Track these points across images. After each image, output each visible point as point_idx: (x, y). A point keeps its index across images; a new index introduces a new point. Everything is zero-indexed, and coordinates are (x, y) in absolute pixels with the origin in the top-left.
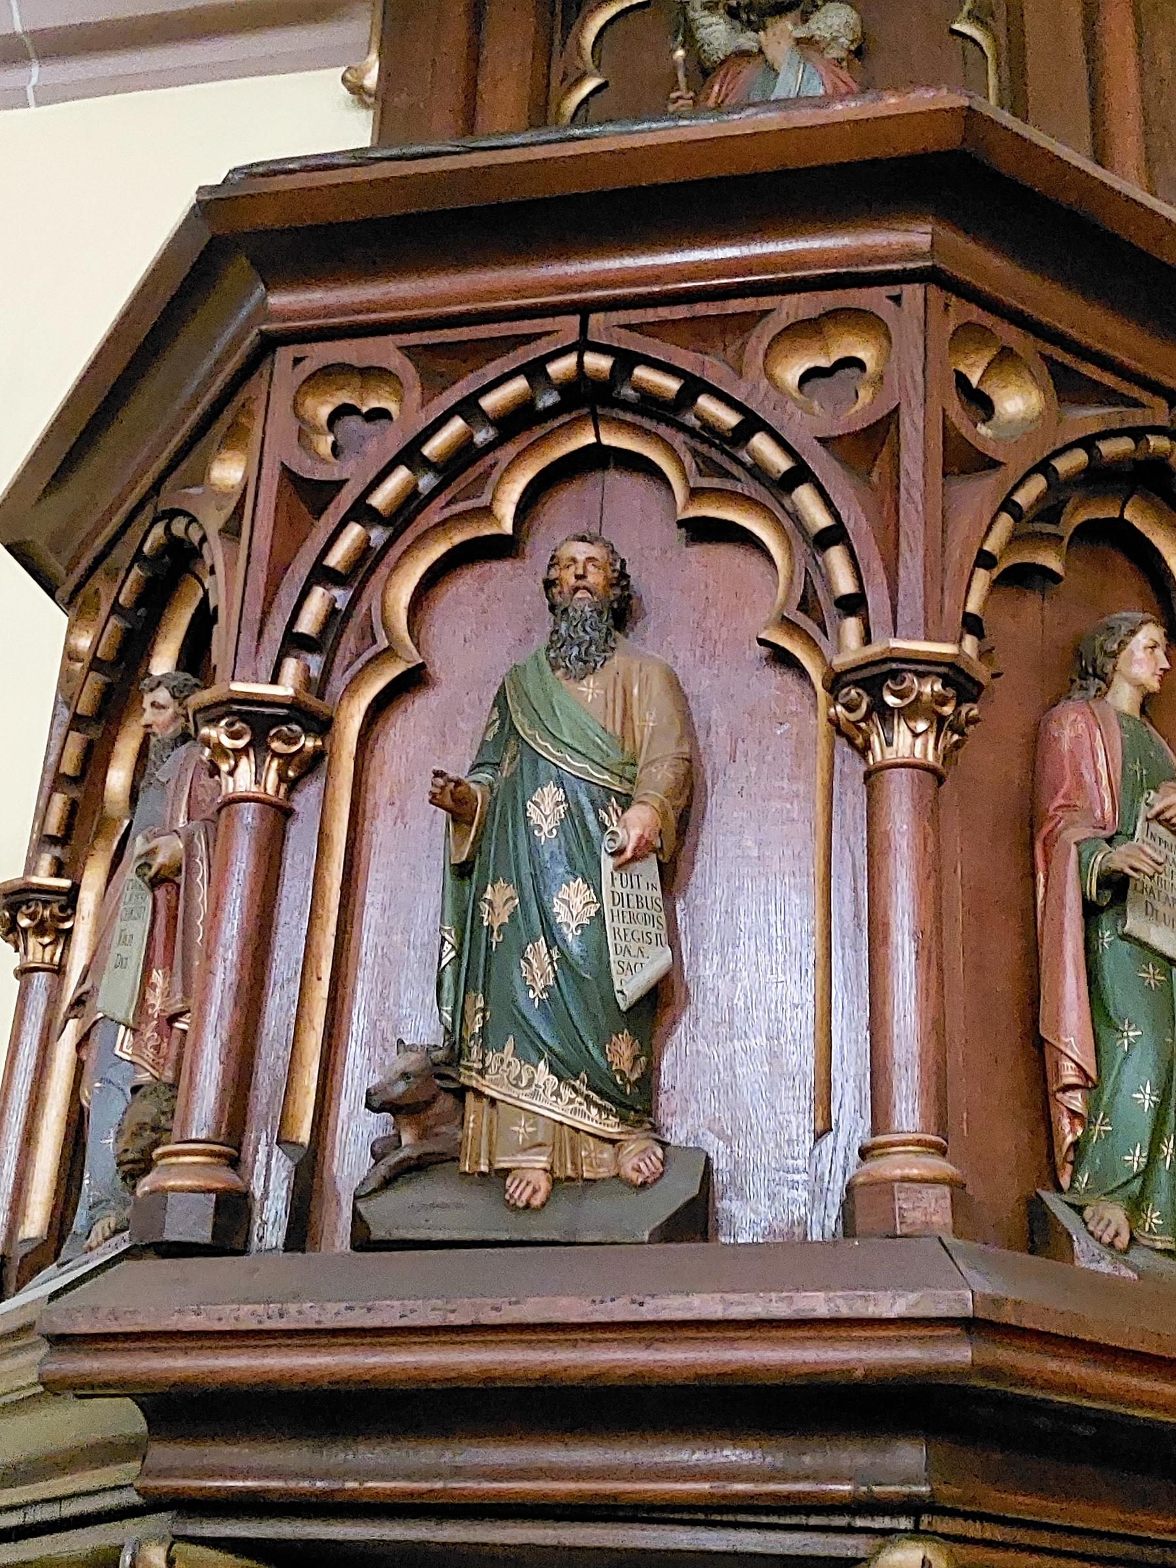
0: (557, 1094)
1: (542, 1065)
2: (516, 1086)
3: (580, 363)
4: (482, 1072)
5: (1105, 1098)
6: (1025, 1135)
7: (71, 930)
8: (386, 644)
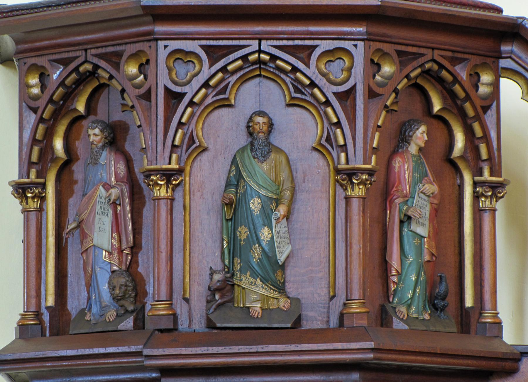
0: (262, 287)
1: (258, 279)
2: (251, 285)
4: (241, 280)
5: (403, 278)
6: (381, 288)
7: (45, 196)
8: (198, 144)
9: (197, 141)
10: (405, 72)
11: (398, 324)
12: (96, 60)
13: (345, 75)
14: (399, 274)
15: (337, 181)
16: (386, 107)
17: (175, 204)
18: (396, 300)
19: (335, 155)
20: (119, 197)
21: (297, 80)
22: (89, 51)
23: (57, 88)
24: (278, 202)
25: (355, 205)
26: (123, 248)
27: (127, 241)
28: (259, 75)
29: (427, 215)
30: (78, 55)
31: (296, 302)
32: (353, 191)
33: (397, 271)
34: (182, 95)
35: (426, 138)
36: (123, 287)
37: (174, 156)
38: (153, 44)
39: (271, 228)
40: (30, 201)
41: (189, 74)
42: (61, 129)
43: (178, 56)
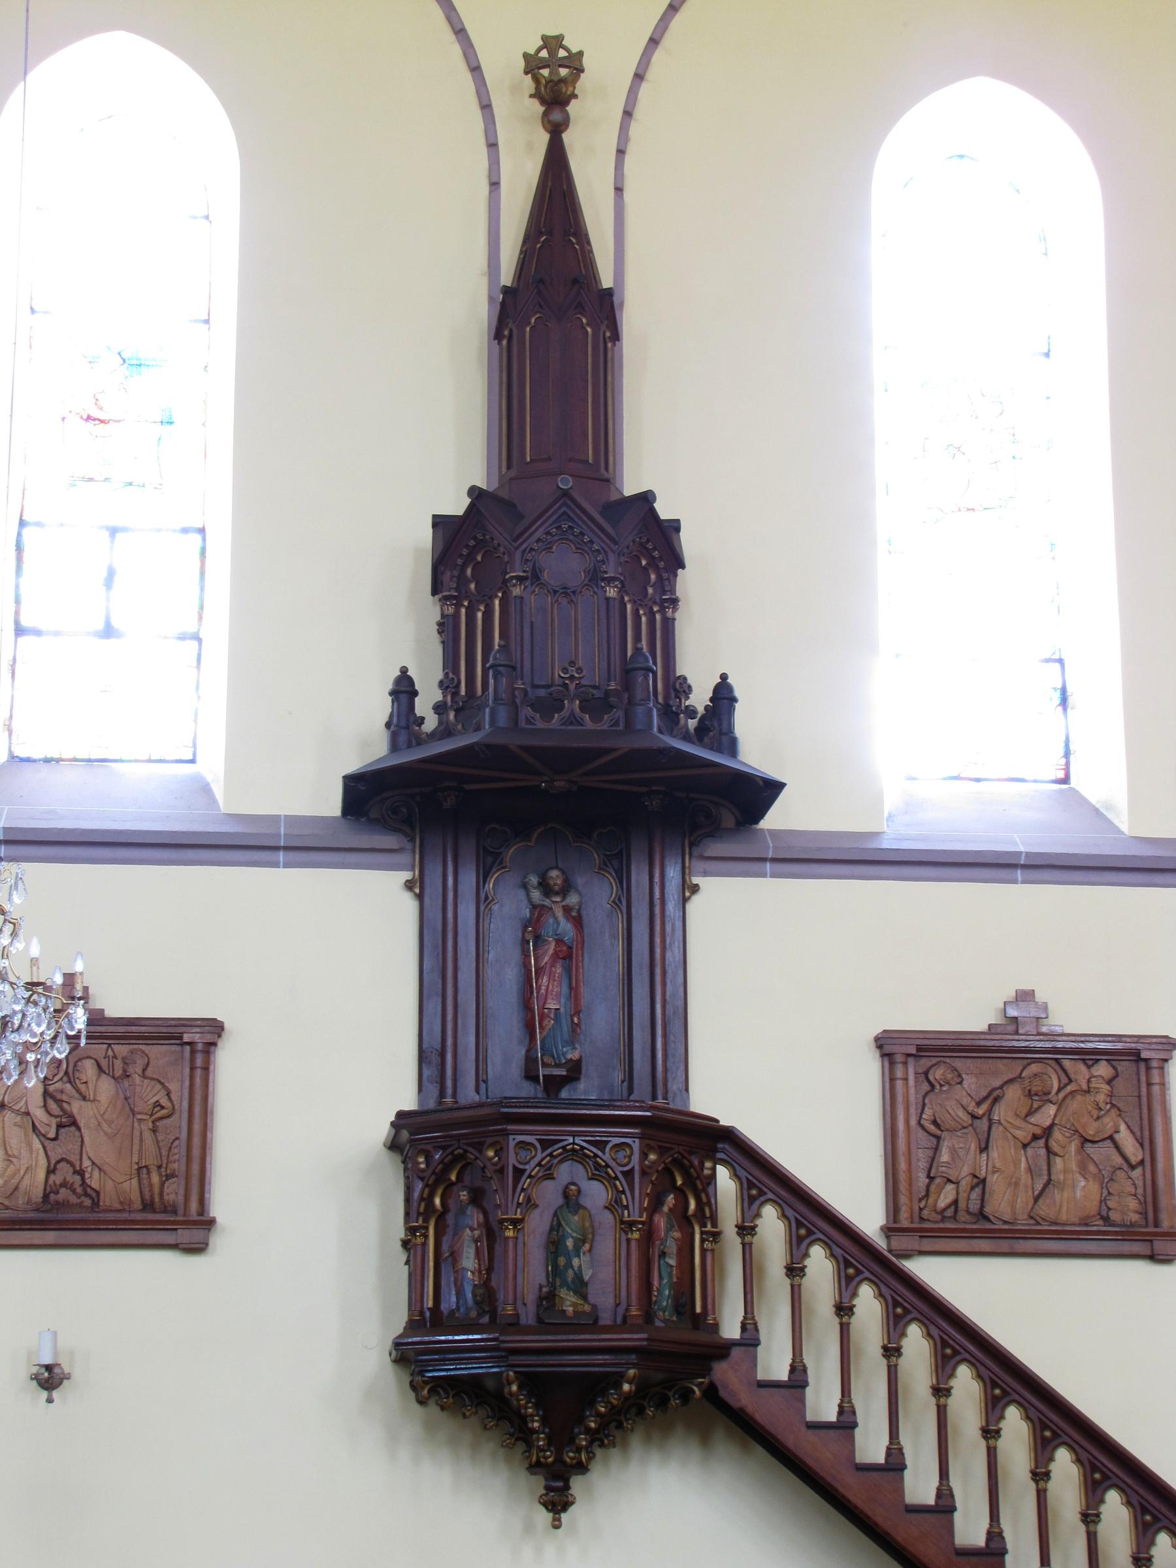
10: (662, 1160)
11: (658, 1323)
12: (465, 1147)
13: (626, 1160)
14: (658, 1290)
15: (621, 1229)
16: (652, 1181)
17: (519, 1241)
18: (656, 1307)
19: (620, 1212)
21: (597, 1163)
23: (439, 1164)
24: (584, 1241)
25: (634, 1245)
27: (485, 1265)
28: (572, 1159)
29: (675, 1252)
31: (594, 1307)
34: (524, 1170)
37: (519, 1210)
38: (506, 1137)
39: (580, 1259)
41: (528, 1158)
42: (439, 1192)
43: (521, 1145)
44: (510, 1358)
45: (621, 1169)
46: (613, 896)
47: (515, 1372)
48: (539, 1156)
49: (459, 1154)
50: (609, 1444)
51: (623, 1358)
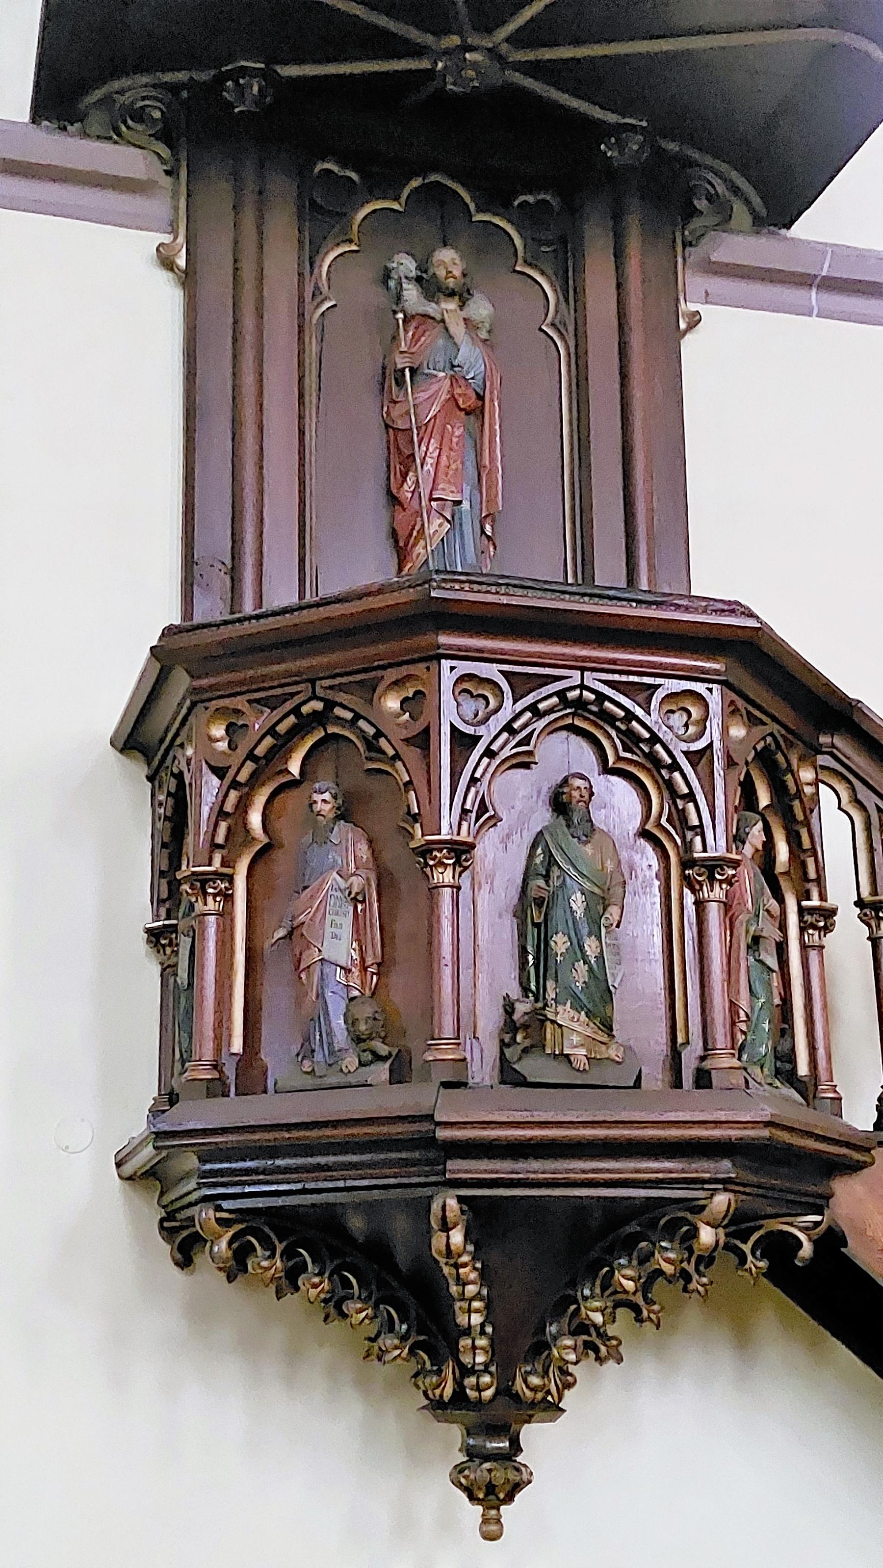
3: (581, 693)
4: (557, 1013)
7: (232, 894)
8: (493, 813)
9: (490, 808)
20: (363, 889)
22: (318, 683)
26: (368, 963)
30: (299, 689)
32: (712, 891)
33: (747, 1016)
34: (476, 739)
35: (765, 839)
36: (369, 1021)
38: (435, 662)
39: (599, 938)
40: (210, 899)
43: (466, 685)
44: (451, 1165)
45: (684, 746)
46: (550, 315)
47: (461, 1199)
48: (508, 710)
49: (315, 712)
50: (609, 1355)
51: (704, 1168)
